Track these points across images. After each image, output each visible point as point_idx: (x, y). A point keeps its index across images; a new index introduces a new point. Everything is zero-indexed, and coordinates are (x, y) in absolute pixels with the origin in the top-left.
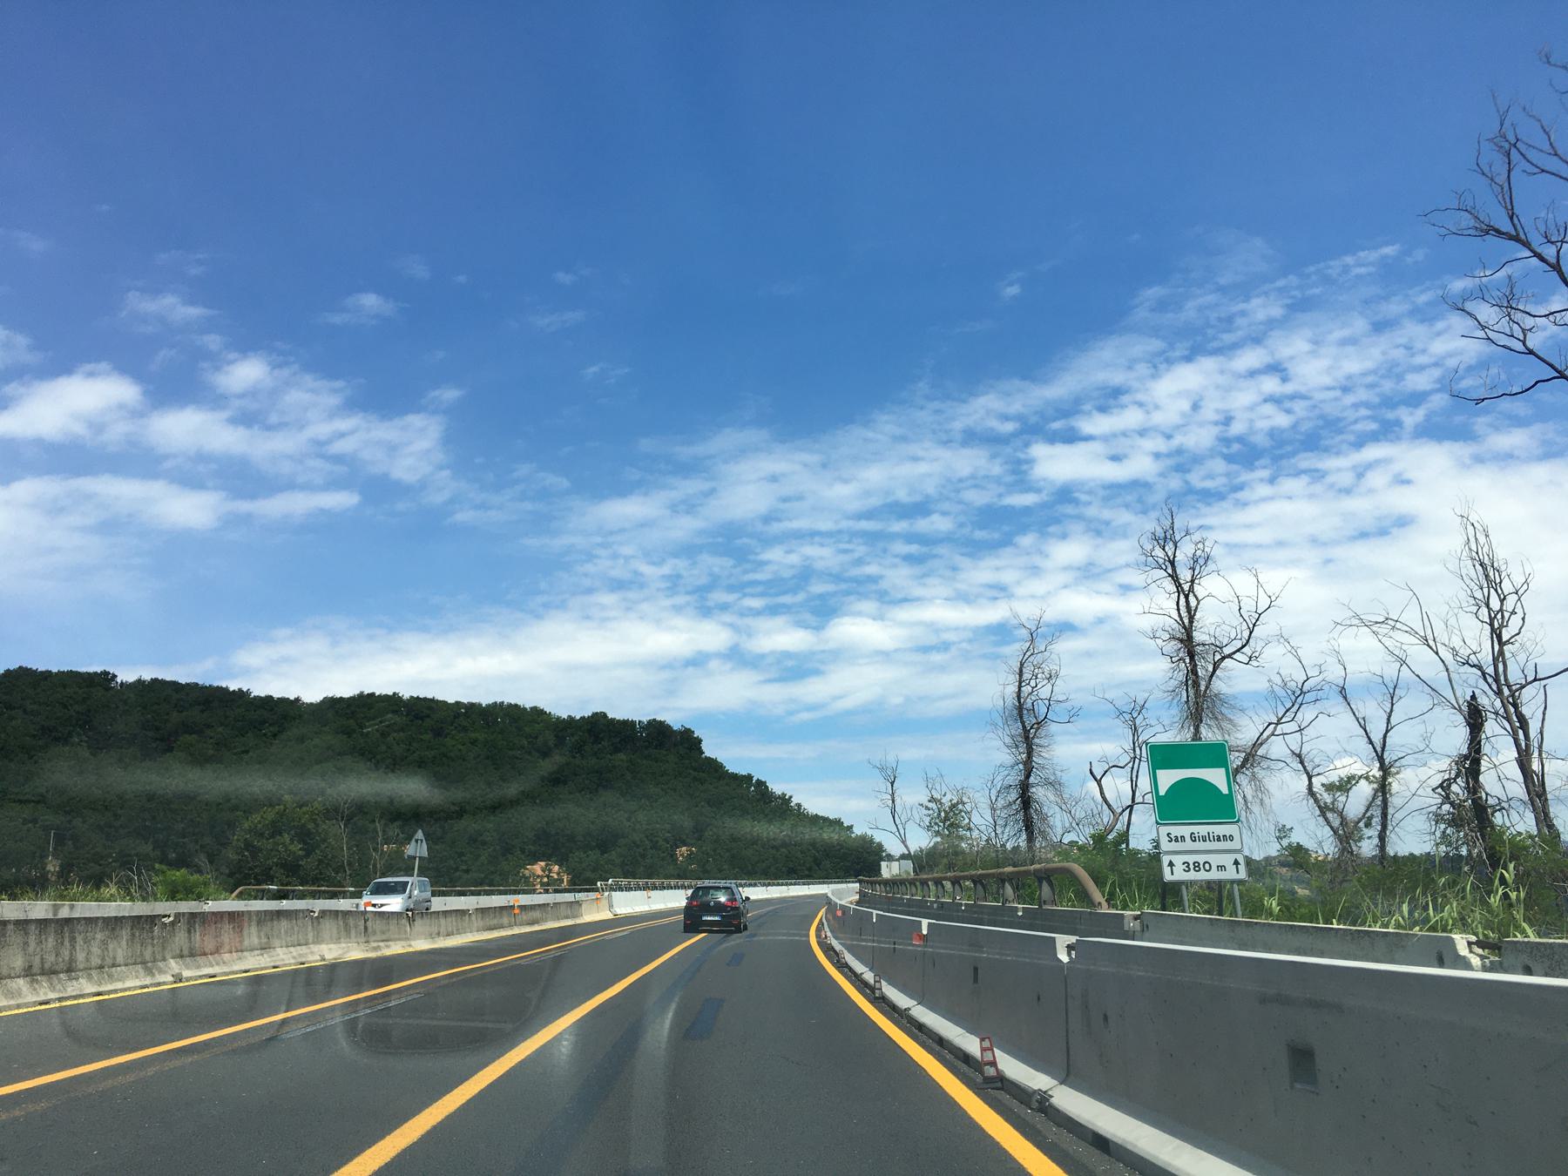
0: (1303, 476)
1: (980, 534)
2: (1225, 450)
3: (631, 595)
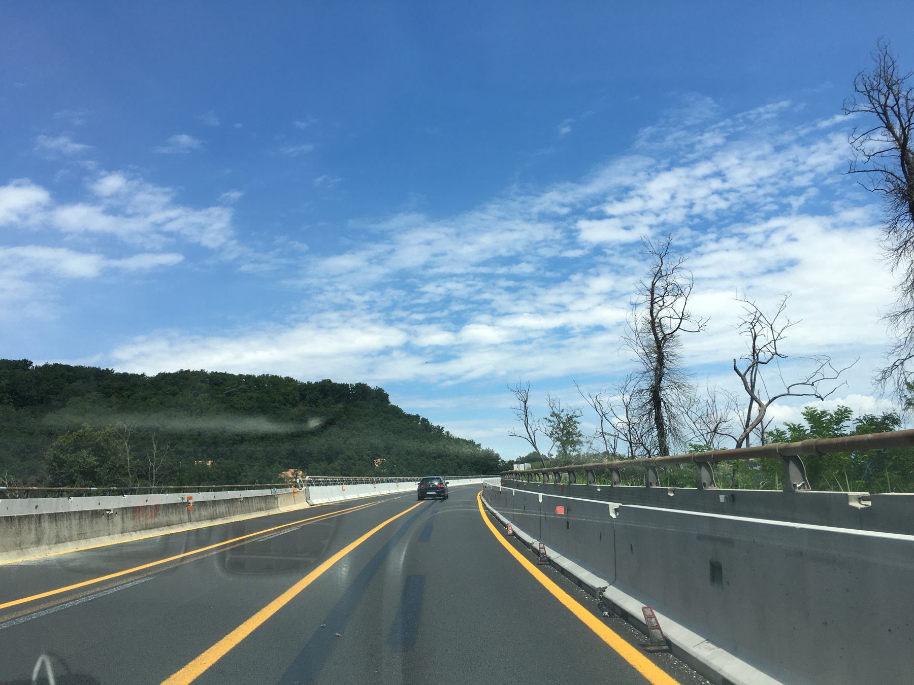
0: (735, 237)
1: (549, 274)
2: (690, 223)
3: (347, 313)
